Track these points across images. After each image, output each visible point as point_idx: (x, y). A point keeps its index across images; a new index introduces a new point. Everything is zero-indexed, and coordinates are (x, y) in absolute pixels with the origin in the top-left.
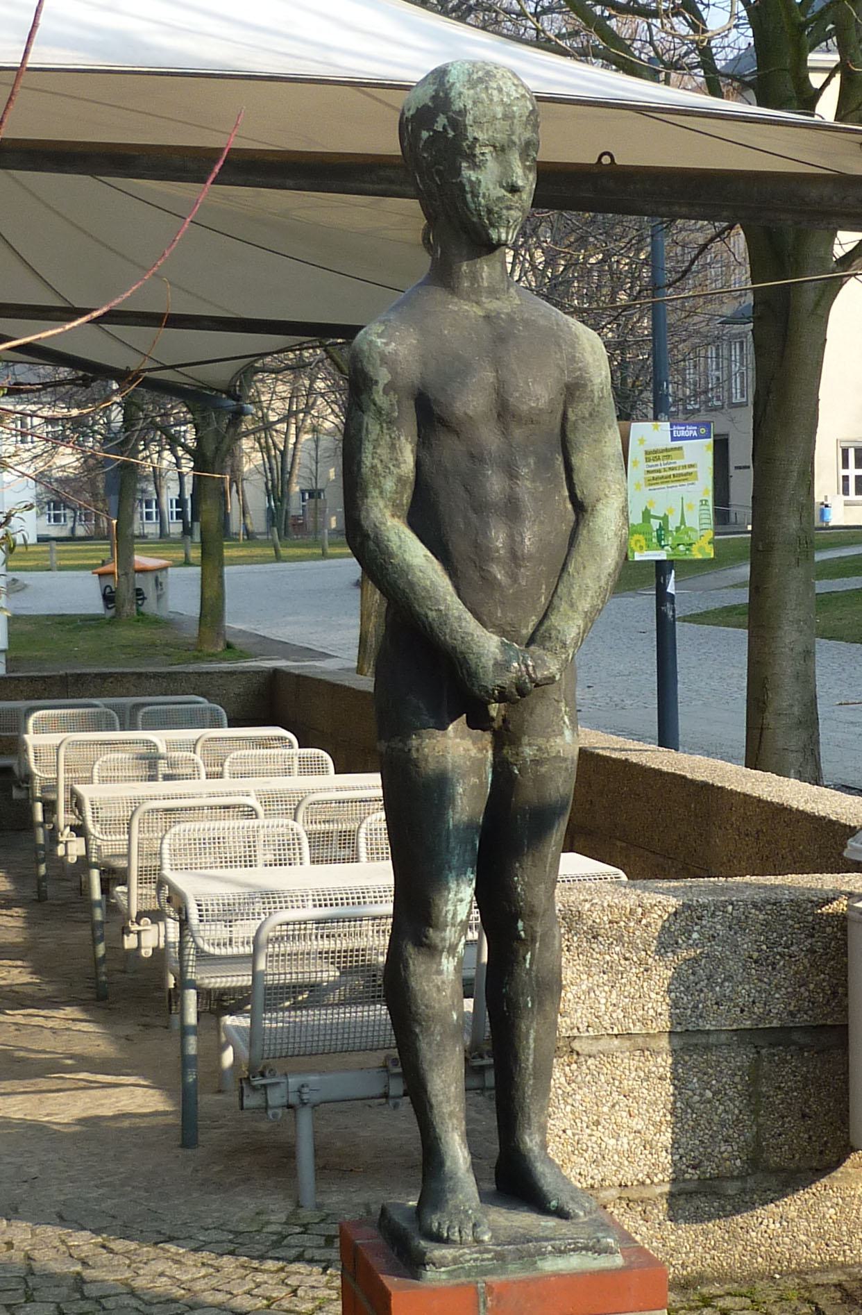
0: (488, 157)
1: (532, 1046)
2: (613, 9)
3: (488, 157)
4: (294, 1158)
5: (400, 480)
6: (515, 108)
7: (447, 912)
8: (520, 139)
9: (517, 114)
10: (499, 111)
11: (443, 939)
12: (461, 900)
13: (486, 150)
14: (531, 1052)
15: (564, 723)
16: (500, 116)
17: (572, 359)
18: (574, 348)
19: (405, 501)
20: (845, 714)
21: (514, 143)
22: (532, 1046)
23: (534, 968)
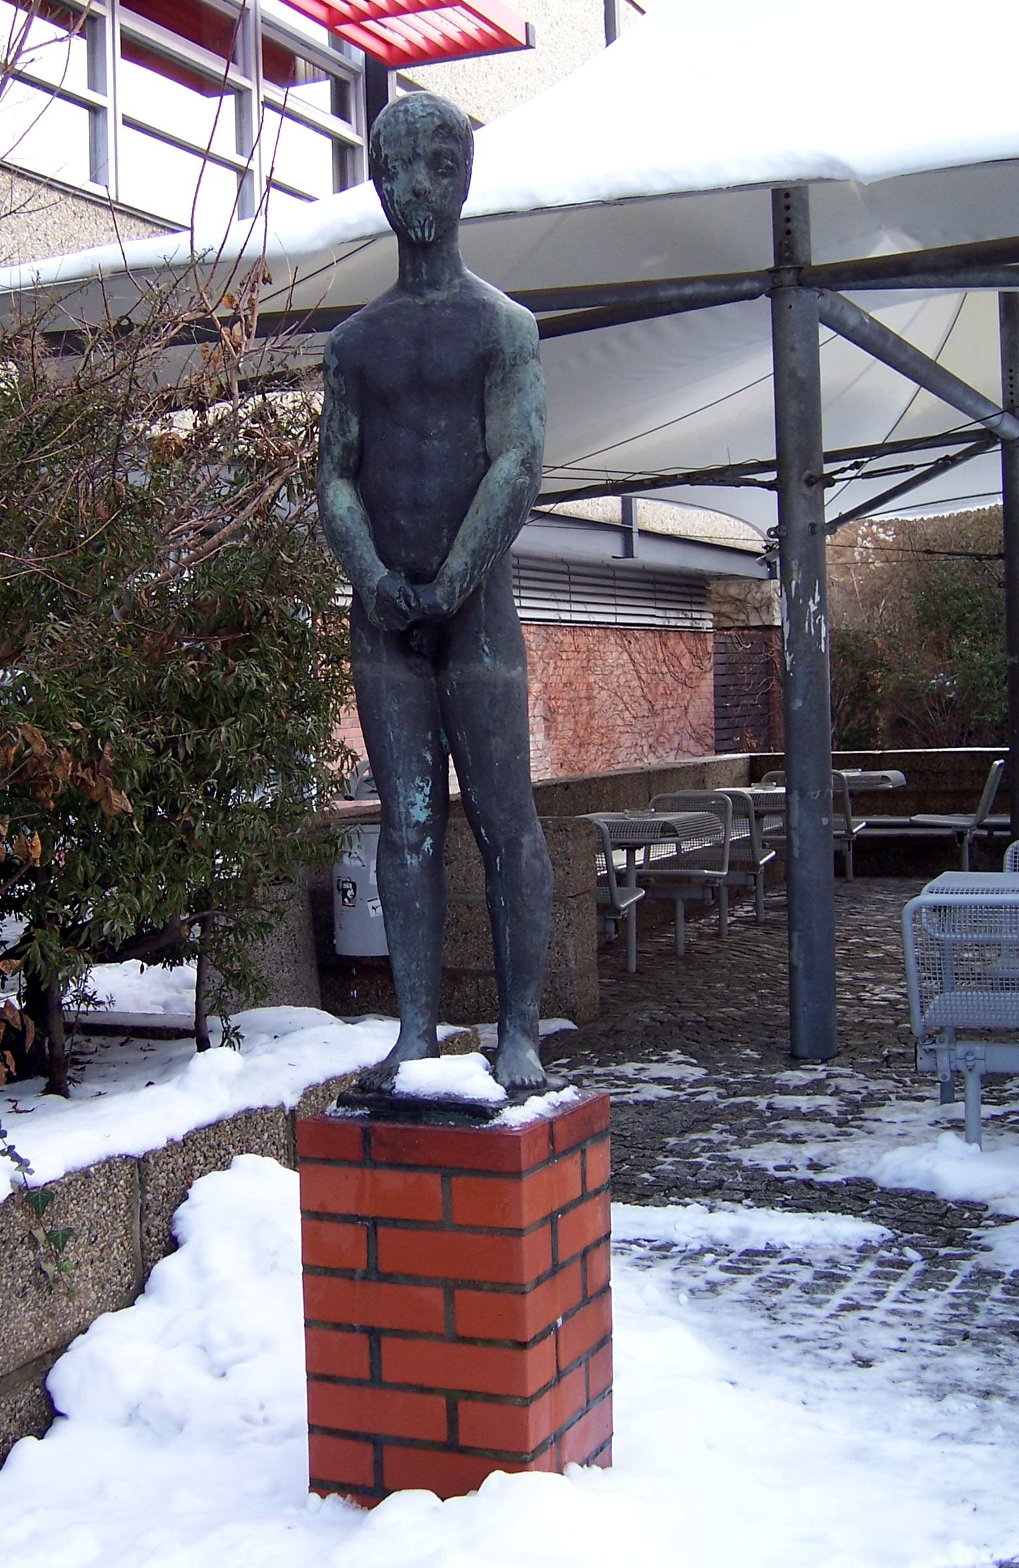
0: (399, 169)
1: (508, 940)
2: (888, 791)
3: (399, 169)
4: (131, 1090)
5: (345, 447)
6: (418, 125)
7: (400, 813)
8: (425, 151)
9: (421, 129)
10: (403, 128)
11: (401, 837)
12: (413, 804)
13: (396, 164)
14: (508, 945)
15: (484, 651)
16: (403, 133)
17: (488, 333)
18: (491, 324)
19: (351, 465)
20: (461, 68)
21: (419, 154)
22: (508, 940)
23: (504, 871)
